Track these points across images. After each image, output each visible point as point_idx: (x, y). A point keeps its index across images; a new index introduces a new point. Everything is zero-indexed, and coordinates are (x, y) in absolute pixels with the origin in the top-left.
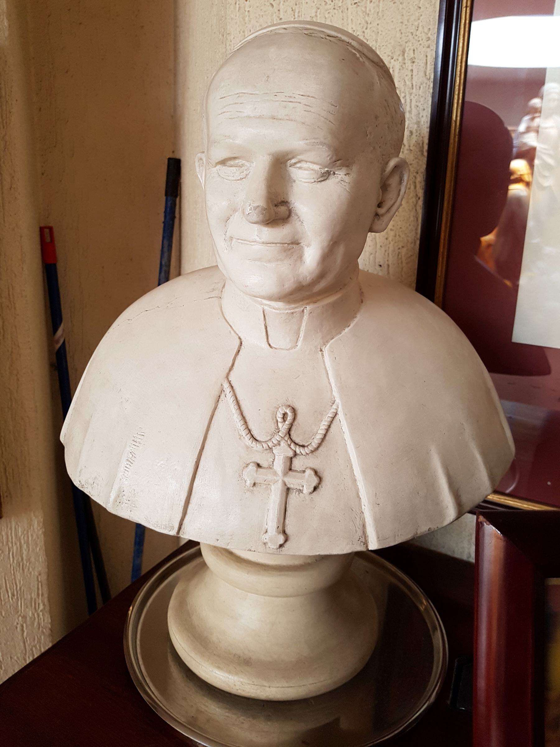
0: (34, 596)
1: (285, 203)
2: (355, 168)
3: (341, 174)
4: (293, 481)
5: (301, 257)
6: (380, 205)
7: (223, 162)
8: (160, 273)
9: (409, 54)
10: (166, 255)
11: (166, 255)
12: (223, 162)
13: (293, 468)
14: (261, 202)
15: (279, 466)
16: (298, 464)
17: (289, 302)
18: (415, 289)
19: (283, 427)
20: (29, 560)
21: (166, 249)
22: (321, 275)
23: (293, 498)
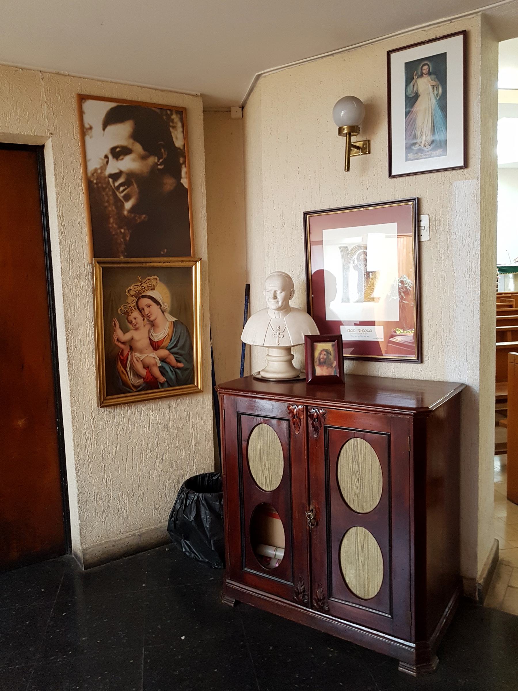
0: (209, 424)
1: (276, 296)
2: (285, 292)
3: (283, 292)
4: (280, 336)
5: (279, 304)
6: (290, 296)
7: (268, 292)
8: (244, 321)
9: (302, 266)
10: (246, 314)
11: (246, 314)
12: (268, 292)
13: (283, 353)
14: (273, 297)
15: (278, 334)
16: (280, 334)
17: (278, 311)
18: (379, 342)
19: (278, 329)
20: (208, 411)
21: (246, 313)
22: (282, 306)
23: (280, 338)
